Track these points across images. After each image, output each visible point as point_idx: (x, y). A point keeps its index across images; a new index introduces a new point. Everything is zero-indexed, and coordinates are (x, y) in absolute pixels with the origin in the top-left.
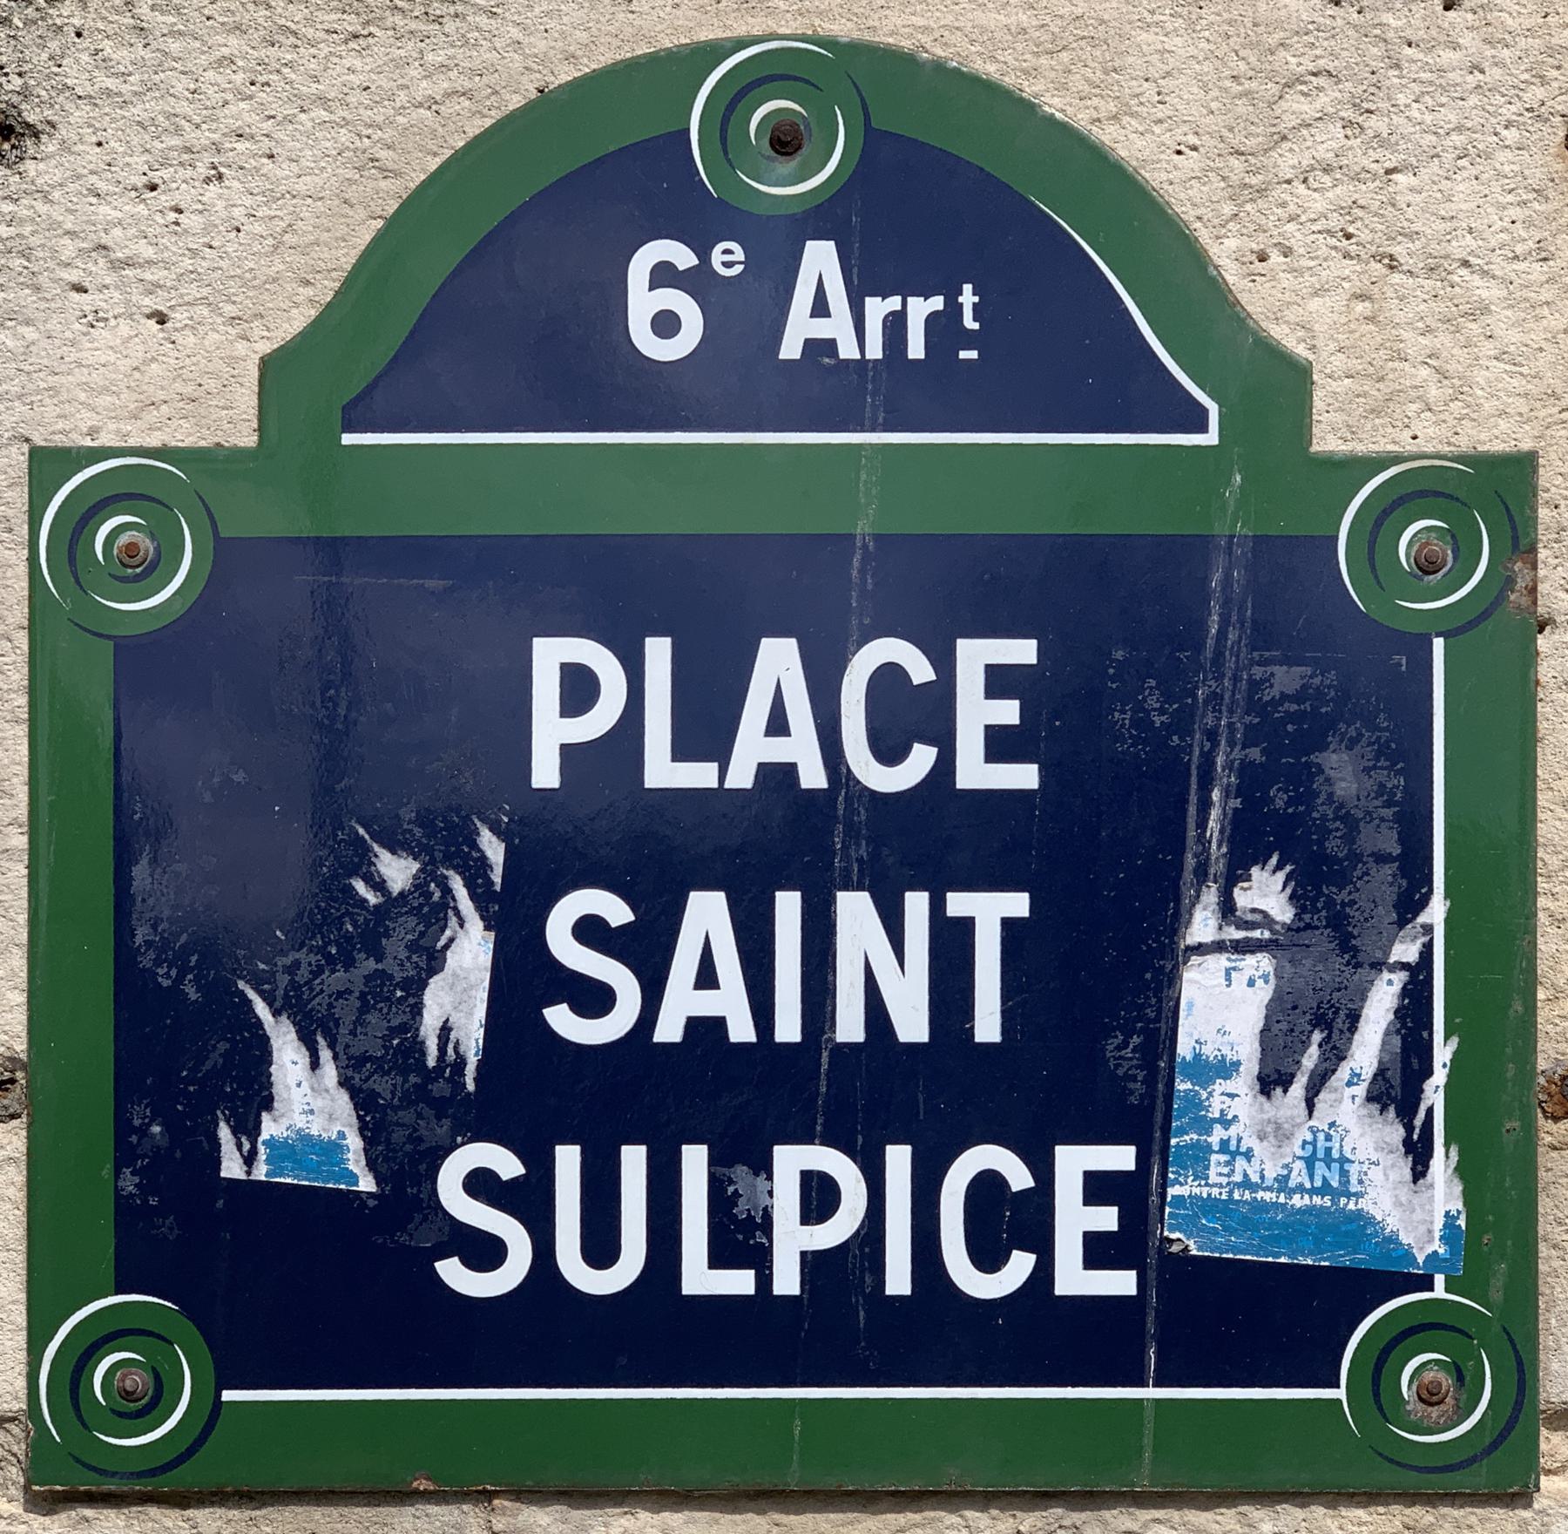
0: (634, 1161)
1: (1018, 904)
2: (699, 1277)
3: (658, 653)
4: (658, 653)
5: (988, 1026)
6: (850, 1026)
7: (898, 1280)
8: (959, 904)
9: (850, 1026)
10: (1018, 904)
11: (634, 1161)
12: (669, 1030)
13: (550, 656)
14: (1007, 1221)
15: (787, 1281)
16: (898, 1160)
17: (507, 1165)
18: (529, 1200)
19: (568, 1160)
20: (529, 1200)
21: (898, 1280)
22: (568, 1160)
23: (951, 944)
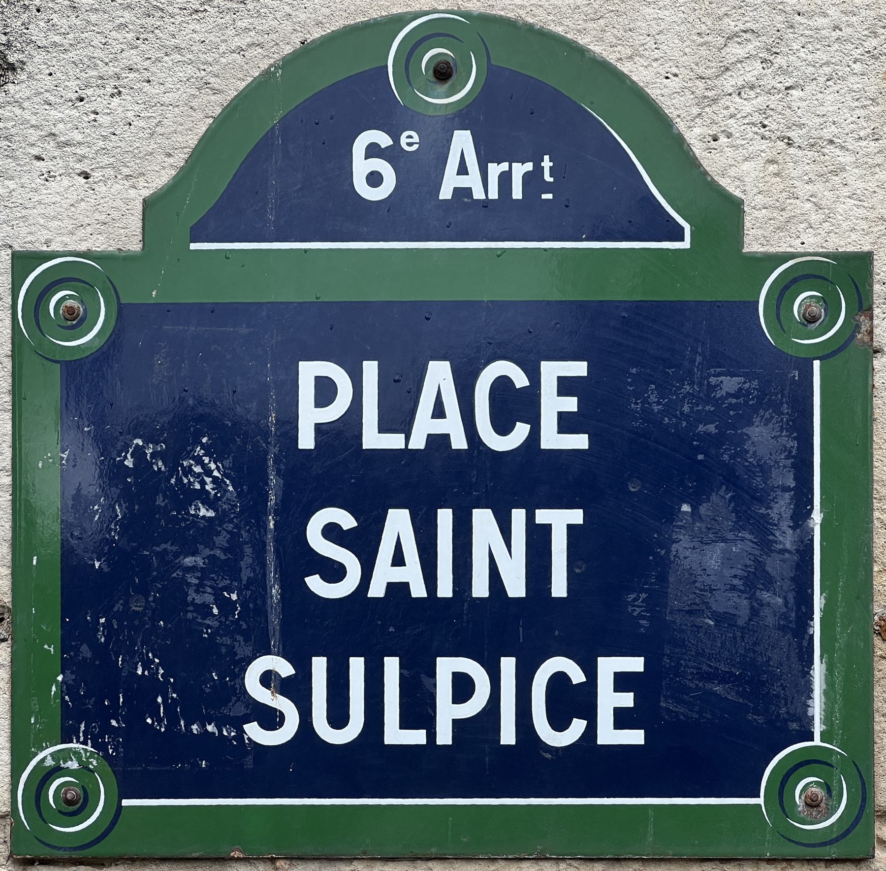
0: (357, 666)
1: (576, 516)
2: (395, 734)
3: (370, 369)
4: (370, 369)
5: (559, 588)
6: (480, 588)
7: (508, 736)
8: (542, 516)
9: (480, 588)
10: (576, 516)
11: (357, 666)
12: (377, 590)
13: (309, 372)
14: (570, 701)
15: (444, 736)
16: (508, 665)
17: (285, 669)
18: (297, 689)
19: (319, 665)
20: (297, 689)
21: (508, 736)
22: (319, 665)
23: (539, 538)
